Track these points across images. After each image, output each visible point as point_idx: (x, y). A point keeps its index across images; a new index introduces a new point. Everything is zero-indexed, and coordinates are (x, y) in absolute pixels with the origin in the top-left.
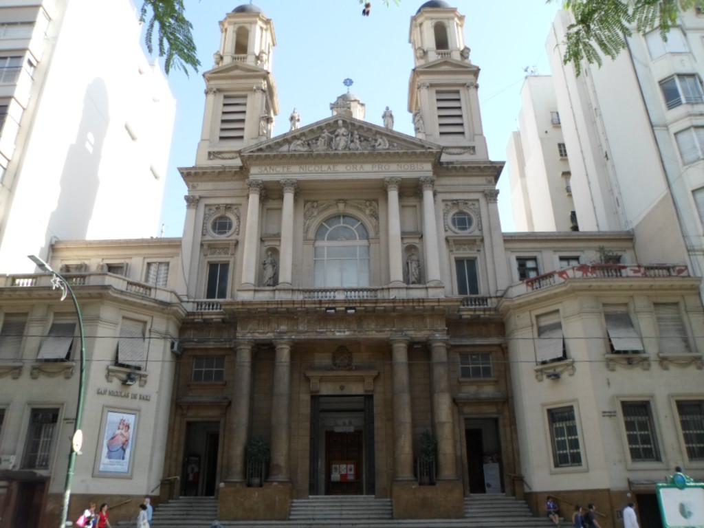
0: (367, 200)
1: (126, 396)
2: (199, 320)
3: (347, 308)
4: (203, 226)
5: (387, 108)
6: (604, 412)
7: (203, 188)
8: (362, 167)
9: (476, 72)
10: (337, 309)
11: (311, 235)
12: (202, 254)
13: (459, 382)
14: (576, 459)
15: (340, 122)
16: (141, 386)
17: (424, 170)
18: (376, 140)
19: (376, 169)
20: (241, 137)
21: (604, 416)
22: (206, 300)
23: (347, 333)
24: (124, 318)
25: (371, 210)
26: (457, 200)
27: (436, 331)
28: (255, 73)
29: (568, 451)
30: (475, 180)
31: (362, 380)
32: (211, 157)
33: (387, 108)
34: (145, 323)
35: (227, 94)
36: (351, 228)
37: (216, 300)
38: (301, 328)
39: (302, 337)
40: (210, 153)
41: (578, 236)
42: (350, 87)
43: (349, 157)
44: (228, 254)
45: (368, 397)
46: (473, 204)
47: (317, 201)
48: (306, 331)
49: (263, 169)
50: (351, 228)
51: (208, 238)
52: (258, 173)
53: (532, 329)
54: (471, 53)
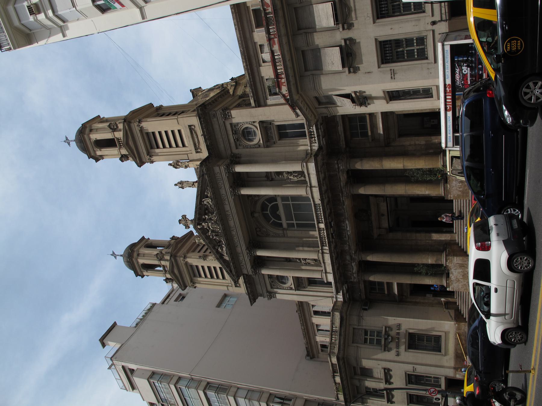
1: (398, 338)
2: (347, 295)
3: (331, 227)
4: (286, 289)
6: (392, 78)
7: (261, 290)
8: (228, 211)
10: (332, 232)
11: (280, 232)
12: (274, 145)
13: (372, 140)
15: (199, 227)
16: (392, 330)
17: (220, 171)
19: (227, 202)
20: (179, 131)
21: (394, 79)
22: (307, 137)
23: (347, 222)
30: (216, 126)
32: (199, 150)
33: (176, 185)
34: (354, 328)
35: (192, 276)
36: (269, 213)
37: (306, 130)
38: (347, 248)
40: (236, 286)
41: (249, 74)
43: (223, 219)
44: (270, 127)
47: (256, 229)
48: (350, 245)
50: (269, 213)
51: (293, 286)
53: (329, 107)
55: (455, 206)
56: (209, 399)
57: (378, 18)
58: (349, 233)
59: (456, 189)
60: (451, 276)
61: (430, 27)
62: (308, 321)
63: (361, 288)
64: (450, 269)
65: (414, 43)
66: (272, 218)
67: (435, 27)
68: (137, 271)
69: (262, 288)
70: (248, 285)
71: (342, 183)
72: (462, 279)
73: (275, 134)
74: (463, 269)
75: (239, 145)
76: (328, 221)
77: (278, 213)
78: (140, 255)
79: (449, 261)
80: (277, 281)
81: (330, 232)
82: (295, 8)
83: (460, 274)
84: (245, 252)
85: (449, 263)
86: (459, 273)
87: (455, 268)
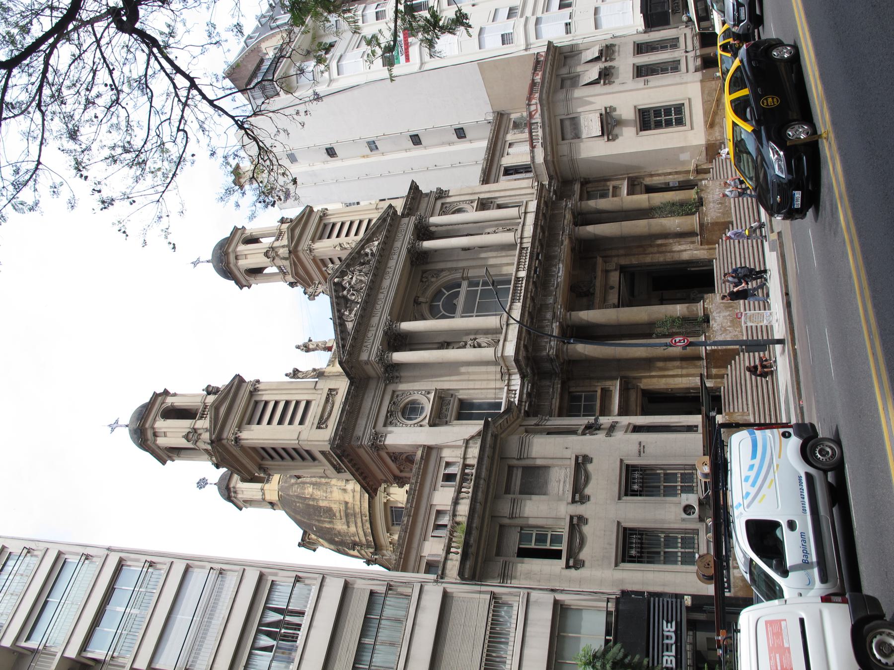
0: (421, 281)
3: (537, 258)
5: (298, 347)
9: (239, 380)
14: (679, 109)
18: (367, 255)
19: (395, 257)
23: (561, 265)
24: (563, 139)
25: (433, 277)
26: (388, 412)
27: (566, 205)
28: (234, 387)
29: (673, 117)
31: (606, 272)
39: (560, 300)
42: (208, 482)
45: (623, 269)
46: (397, 396)
49: (365, 348)
52: (371, 351)
54: (213, 385)
55: (717, 272)
56: (114, 589)
57: (623, 561)
58: (559, 280)
59: (715, 211)
60: (713, 324)
61: (685, 54)
62: (496, 159)
63: (553, 407)
64: (711, 312)
65: (677, 543)
66: (442, 310)
67: (687, 54)
68: (148, 420)
69: (366, 425)
70: (347, 407)
71: (566, 222)
72: (730, 327)
73: (453, 408)
74: (730, 311)
75: (391, 422)
76: (536, 250)
77: (455, 302)
78: (239, 257)
79: (708, 301)
80: (400, 414)
81: (534, 264)
82: (502, 526)
83: (726, 319)
84: (385, 316)
85: (707, 304)
86: (724, 317)
87: (718, 310)
